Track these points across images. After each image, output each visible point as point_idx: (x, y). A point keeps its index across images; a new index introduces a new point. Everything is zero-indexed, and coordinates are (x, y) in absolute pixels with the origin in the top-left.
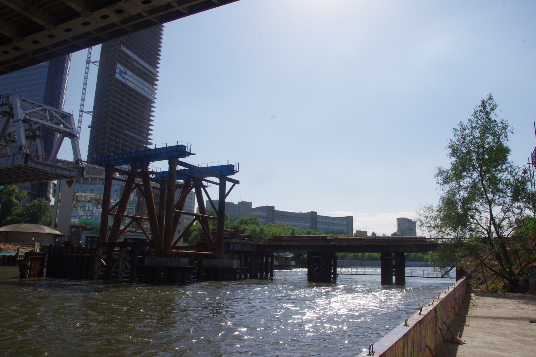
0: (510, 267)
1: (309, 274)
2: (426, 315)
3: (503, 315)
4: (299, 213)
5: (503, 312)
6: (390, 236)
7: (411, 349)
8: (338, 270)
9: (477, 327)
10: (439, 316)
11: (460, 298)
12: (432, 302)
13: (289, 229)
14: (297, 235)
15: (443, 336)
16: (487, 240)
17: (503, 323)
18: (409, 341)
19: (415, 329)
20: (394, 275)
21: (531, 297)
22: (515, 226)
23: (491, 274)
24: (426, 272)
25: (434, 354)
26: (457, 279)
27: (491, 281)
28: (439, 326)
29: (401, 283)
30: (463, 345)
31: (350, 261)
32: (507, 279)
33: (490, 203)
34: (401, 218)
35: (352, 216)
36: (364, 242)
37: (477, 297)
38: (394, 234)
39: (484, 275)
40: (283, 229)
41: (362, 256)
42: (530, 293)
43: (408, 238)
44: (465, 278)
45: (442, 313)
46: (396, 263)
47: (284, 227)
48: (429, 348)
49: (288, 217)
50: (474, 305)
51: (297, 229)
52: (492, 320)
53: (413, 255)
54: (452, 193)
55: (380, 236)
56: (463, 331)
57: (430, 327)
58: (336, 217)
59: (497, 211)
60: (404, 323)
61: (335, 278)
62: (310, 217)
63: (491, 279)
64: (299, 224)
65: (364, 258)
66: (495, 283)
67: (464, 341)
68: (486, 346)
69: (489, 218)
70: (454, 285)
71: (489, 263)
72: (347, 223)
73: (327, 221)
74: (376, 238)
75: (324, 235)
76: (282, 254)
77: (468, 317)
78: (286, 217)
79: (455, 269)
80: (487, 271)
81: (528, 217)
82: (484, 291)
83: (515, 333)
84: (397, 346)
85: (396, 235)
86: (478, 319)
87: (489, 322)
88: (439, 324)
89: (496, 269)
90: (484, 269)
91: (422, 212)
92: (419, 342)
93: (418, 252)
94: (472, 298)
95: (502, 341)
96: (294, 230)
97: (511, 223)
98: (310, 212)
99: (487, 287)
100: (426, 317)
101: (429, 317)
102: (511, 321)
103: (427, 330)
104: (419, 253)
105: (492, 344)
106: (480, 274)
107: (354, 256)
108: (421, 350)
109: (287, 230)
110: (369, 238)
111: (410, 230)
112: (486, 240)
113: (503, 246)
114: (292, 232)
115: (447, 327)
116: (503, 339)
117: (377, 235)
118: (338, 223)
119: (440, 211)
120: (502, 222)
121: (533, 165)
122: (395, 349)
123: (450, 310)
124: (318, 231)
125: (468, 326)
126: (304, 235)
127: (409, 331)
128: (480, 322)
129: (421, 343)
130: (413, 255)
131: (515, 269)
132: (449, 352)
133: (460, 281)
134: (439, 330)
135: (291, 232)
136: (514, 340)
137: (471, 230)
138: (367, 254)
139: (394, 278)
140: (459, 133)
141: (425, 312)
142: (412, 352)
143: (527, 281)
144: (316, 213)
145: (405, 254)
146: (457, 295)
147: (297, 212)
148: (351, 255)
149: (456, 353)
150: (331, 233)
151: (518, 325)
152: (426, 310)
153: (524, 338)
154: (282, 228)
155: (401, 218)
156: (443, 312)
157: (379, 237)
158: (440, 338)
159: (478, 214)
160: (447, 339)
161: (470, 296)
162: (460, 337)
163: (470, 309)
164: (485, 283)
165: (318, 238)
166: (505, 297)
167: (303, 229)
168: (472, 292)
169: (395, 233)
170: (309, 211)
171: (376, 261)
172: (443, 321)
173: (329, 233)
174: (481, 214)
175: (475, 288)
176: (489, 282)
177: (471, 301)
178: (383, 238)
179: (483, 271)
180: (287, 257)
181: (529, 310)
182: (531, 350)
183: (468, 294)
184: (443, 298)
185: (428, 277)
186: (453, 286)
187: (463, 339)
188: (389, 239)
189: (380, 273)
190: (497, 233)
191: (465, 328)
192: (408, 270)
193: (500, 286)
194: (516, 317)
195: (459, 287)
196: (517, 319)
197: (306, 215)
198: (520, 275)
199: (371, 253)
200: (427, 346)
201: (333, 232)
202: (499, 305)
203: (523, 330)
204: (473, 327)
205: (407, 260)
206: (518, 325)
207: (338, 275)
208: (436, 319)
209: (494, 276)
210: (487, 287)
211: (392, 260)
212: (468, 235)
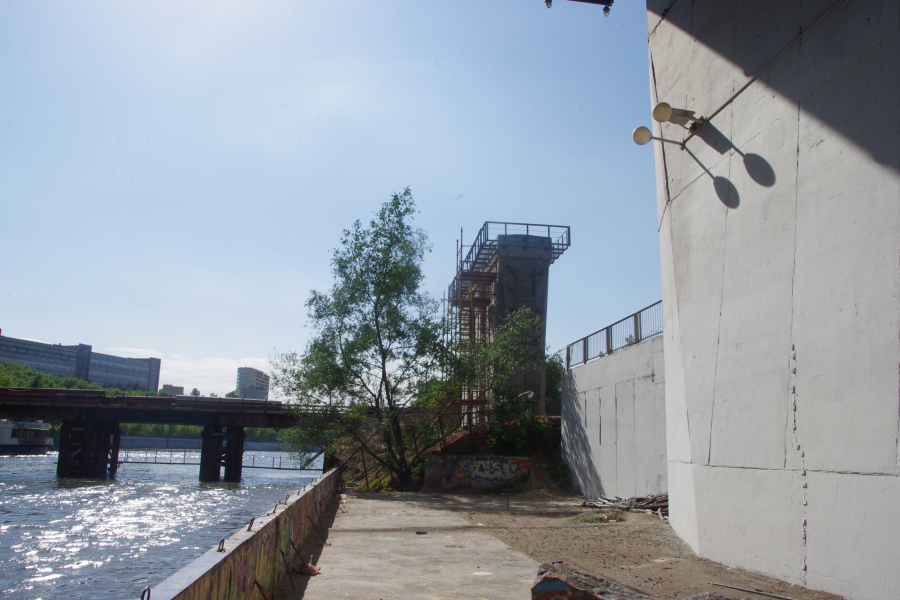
0: (402, 453)
1: (61, 463)
2: (258, 532)
3: (383, 526)
4: (54, 345)
5: (382, 522)
8: (122, 455)
9: (343, 546)
10: (283, 533)
11: (323, 501)
13: (29, 374)
14: (45, 387)
15: (287, 566)
16: (374, 411)
17: (381, 537)
18: (222, 577)
19: (236, 555)
20: (223, 464)
21: (426, 497)
22: (417, 391)
23: (375, 463)
24: (277, 461)
25: (268, 595)
26: (324, 471)
27: (374, 474)
28: (282, 549)
29: (234, 479)
30: (317, 575)
32: (396, 471)
33: (385, 354)
34: (246, 368)
35: (159, 358)
36: (176, 406)
37: (350, 500)
38: (232, 394)
40: (16, 374)
41: (172, 431)
42: (424, 492)
43: (253, 403)
45: (289, 526)
47: (18, 371)
48: (259, 586)
49: (30, 352)
50: (344, 513)
51: (45, 376)
53: (258, 432)
54: (331, 334)
55: (206, 396)
56: (320, 554)
59: (394, 367)
60: (217, 547)
61: (113, 470)
63: (374, 472)
64: (52, 366)
68: (351, 574)
70: (316, 482)
71: (373, 447)
73: (111, 364)
76: (28, 425)
77: (332, 531)
78: (24, 351)
79: (323, 455)
81: (434, 379)
82: (363, 490)
83: (394, 551)
85: (234, 397)
86: (346, 533)
87: (364, 536)
88: (283, 545)
91: (278, 361)
94: (342, 501)
96: (39, 377)
98: (78, 344)
99: (367, 483)
100: (259, 533)
101: (265, 535)
103: (258, 557)
104: (269, 429)
105: (360, 570)
107: (156, 430)
108: (244, 590)
109: (24, 377)
111: (258, 388)
112: (373, 411)
113: (395, 421)
114: (35, 381)
116: (376, 561)
117: (201, 395)
118: (131, 369)
119: (307, 361)
120: (397, 384)
122: (192, 594)
124: (89, 382)
125: (330, 545)
126: (60, 387)
127: (225, 560)
128: (348, 538)
129: (245, 579)
130: (259, 431)
132: (294, 589)
133: (326, 475)
135: (33, 380)
137: (353, 393)
138: (180, 427)
139: (223, 470)
140: (351, 238)
141: (257, 526)
142: (228, 595)
145: (245, 429)
147: (52, 343)
148: (150, 427)
149: (305, 590)
150: (116, 387)
151: (401, 539)
152: (262, 523)
153: (406, 557)
154: (13, 372)
155: (246, 368)
156: (292, 525)
157: (203, 398)
158: (282, 568)
159: (365, 369)
160: (293, 568)
161: (340, 499)
162: (315, 563)
163: (336, 519)
164: (365, 478)
165: (87, 395)
167: (59, 376)
168: (344, 491)
170: (76, 343)
171: (194, 440)
172: (290, 540)
173: (110, 386)
174: (370, 369)
175: (350, 485)
176: (371, 476)
177: (341, 506)
179: (363, 459)
180: (37, 430)
181: (419, 516)
184: (294, 501)
185: (280, 469)
188: (220, 402)
189: (199, 461)
190: (390, 401)
191: (325, 549)
192: (247, 457)
193: (385, 482)
195: (323, 485)
196: (400, 530)
198: (414, 464)
199: (186, 426)
200: (256, 582)
201: (119, 385)
202: (380, 511)
203: (406, 545)
206: (401, 539)
207: (121, 465)
208: (277, 536)
209: (379, 466)
210: (367, 483)
212: (347, 403)
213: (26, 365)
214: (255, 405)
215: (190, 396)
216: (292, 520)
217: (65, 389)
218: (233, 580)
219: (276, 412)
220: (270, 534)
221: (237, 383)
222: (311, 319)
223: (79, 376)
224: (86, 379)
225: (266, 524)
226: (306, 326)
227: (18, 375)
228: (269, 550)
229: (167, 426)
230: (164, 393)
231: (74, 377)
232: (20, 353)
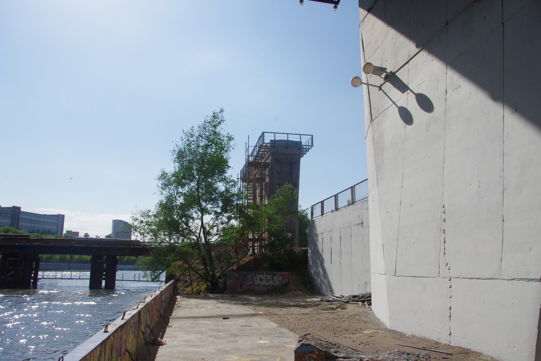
0: (213, 271)
6: (104, 238)
7: (109, 357)
9: (179, 327)
10: (143, 320)
12: (137, 306)
15: (145, 340)
16: (196, 245)
17: (201, 321)
18: (107, 348)
20: (104, 279)
23: (197, 277)
24: (137, 276)
25: (134, 358)
27: (196, 283)
28: (142, 330)
31: (56, 264)
32: (210, 282)
34: (117, 220)
36: (74, 244)
38: (109, 236)
39: (191, 278)
42: (226, 293)
43: (122, 241)
44: (172, 281)
45: (147, 316)
46: (107, 266)
48: (129, 353)
50: (179, 307)
52: (193, 319)
53: (126, 259)
54: (171, 199)
55: (93, 237)
57: (132, 331)
58: (44, 215)
62: (11, 213)
63: (196, 282)
65: (73, 261)
66: (199, 286)
67: (165, 342)
68: (184, 344)
69: (200, 225)
70: (162, 289)
72: (57, 221)
73: (33, 218)
74: (88, 240)
75: (28, 234)
77: (172, 318)
80: (193, 275)
83: (210, 330)
84: (92, 355)
85: (111, 237)
88: (143, 328)
89: (201, 273)
90: (191, 272)
92: (119, 347)
93: (131, 256)
94: (177, 300)
95: (199, 338)
97: (219, 230)
98: (12, 206)
99: (192, 289)
100: (129, 321)
101: (132, 322)
102: (208, 319)
106: (188, 277)
107: (61, 258)
108: (120, 355)
110: (80, 240)
115: (150, 330)
116: (199, 336)
117: (90, 237)
118: (46, 221)
121: (241, 180)
123: (155, 312)
124: (20, 229)
125: (171, 326)
127: (108, 338)
128: (182, 322)
130: (126, 258)
131: (217, 273)
132: (150, 354)
133: (167, 285)
134: (142, 333)
136: (209, 336)
138: (76, 257)
141: (128, 317)
143: (225, 283)
144: (19, 208)
145: (117, 257)
146: (164, 298)
148: (58, 257)
152: (130, 314)
155: (117, 220)
157: (92, 239)
161: (176, 298)
162: (162, 338)
163: (174, 311)
164: (191, 286)
166: (206, 298)
169: (109, 235)
171: (85, 264)
172: (147, 324)
173: (32, 232)
176: (195, 284)
177: (177, 303)
178: (96, 240)
181: (224, 308)
182: (221, 343)
183: (175, 297)
186: (161, 290)
187: (164, 340)
190: (205, 239)
191: (168, 329)
192: (119, 274)
194: (212, 315)
195: (166, 290)
196: (213, 317)
197: (6, 210)
198: (220, 277)
200: (127, 350)
202: (200, 306)
203: (217, 326)
204: (175, 327)
205: (119, 263)
206: (214, 322)
208: (139, 322)
210: (192, 289)
211: (103, 263)
215: (83, 237)
218: (113, 349)
224: (17, 228)
225: (133, 315)
229: (69, 256)
231: (10, 226)
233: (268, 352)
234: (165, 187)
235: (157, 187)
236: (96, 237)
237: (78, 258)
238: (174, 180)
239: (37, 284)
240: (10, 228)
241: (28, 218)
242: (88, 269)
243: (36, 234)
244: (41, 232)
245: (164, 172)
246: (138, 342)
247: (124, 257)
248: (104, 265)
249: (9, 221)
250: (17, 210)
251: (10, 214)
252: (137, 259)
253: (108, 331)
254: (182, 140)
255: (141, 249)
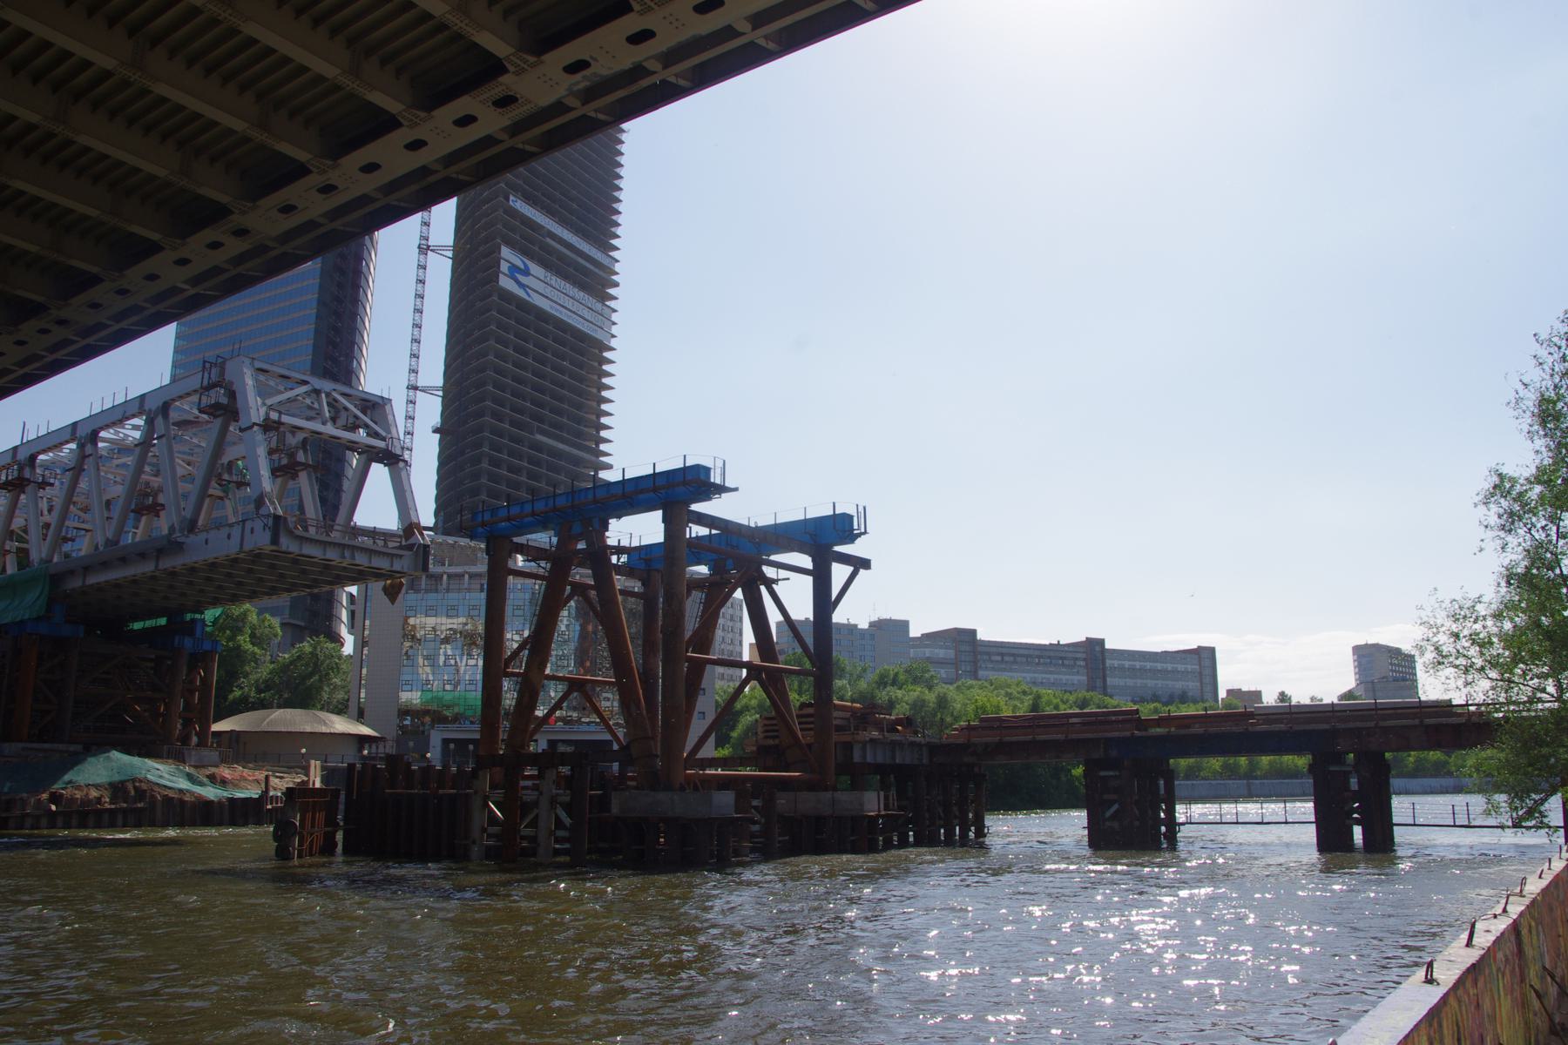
2: (1489, 948)
4: (1051, 644)
8: (1181, 812)
14: (1049, 711)
18: (1445, 1032)
19: (1460, 992)
20: (1358, 822)
38: (1349, 695)
41: (1253, 767)
43: (1395, 707)
45: (1538, 939)
46: (1359, 783)
47: (1009, 690)
51: (1047, 693)
53: (1411, 759)
55: (1302, 702)
62: (1084, 656)
64: (1052, 677)
65: (1259, 773)
73: (1138, 664)
78: (1012, 659)
93: (1430, 748)
96: (1038, 697)
100: (1490, 952)
101: (1500, 955)
103: (1496, 997)
107: (1225, 766)
109: (1018, 698)
111: (1396, 680)
118: (1169, 669)
124: (1111, 697)
127: (1444, 999)
130: (1412, 757)
138: (1265, 760)
139: (1358, 832)
141: (1484, 940)
144: (1101, 642)
145: (1387, 755)
148: (1216, 763)
150: (1153, 701)
154: (1003, 692)
157: (1299, 706)
169: (1350, 691)
172: (1544, 968)
173: (1142, 700)
192: (1401, 806)
197: (1071, 649)
207: (1182, 827)
211: (1345, 776)
213: (1016, 678)
214: (1400, 711)
215: (1274, 704)
216: (1540, 927)
217: (1077, 711)
218: (1463, 1038)
219: (1444, 720)
220: (1508, 952)
221: (1356, 674)
222: (1490, 534)
223: (1091, 688)
224: (1105, 694)
225: (1498, 934)
226: (1481, 550)
227: (1009, 695)
228: (1512, 984)
229: (1243, 758)
230: (1230, 705)
231: (1088, 691)
232: (1007, 662)
233: (275, 1007)
234: (1513, 523)
235: (1483, 528)
236: (1312, 699)
237: (1270, 762)
238: (1541, 497)
239: (1176, 837)
240: (1088, 695)
241: (1061, 680)
242: (1304, 794)
243: (1152, 706)
244: (1164, 700)
245: (1500, 475)
246: (1527, 1023)
247: (1406, 754)
248: (1352, 780)
249: (1085, 678)
250: (1098, 648)
251: (1085, 659)
252: (1450, 757)
253: (1435, 981)
254: (1541, 364)
255: (1460, 725)
